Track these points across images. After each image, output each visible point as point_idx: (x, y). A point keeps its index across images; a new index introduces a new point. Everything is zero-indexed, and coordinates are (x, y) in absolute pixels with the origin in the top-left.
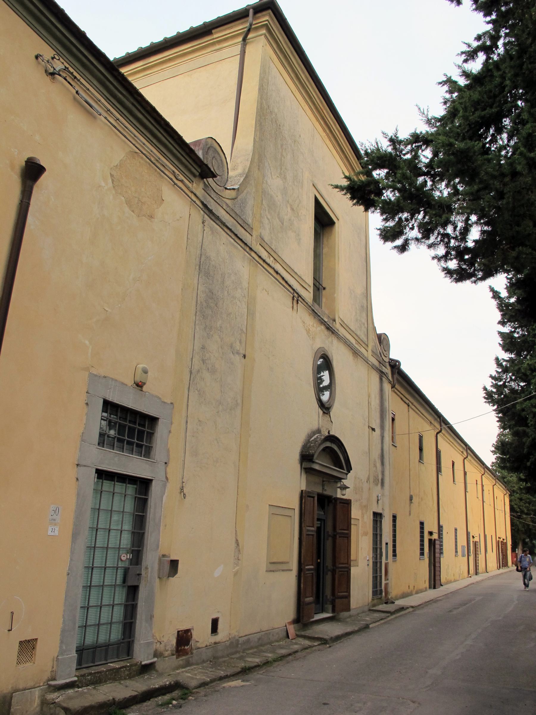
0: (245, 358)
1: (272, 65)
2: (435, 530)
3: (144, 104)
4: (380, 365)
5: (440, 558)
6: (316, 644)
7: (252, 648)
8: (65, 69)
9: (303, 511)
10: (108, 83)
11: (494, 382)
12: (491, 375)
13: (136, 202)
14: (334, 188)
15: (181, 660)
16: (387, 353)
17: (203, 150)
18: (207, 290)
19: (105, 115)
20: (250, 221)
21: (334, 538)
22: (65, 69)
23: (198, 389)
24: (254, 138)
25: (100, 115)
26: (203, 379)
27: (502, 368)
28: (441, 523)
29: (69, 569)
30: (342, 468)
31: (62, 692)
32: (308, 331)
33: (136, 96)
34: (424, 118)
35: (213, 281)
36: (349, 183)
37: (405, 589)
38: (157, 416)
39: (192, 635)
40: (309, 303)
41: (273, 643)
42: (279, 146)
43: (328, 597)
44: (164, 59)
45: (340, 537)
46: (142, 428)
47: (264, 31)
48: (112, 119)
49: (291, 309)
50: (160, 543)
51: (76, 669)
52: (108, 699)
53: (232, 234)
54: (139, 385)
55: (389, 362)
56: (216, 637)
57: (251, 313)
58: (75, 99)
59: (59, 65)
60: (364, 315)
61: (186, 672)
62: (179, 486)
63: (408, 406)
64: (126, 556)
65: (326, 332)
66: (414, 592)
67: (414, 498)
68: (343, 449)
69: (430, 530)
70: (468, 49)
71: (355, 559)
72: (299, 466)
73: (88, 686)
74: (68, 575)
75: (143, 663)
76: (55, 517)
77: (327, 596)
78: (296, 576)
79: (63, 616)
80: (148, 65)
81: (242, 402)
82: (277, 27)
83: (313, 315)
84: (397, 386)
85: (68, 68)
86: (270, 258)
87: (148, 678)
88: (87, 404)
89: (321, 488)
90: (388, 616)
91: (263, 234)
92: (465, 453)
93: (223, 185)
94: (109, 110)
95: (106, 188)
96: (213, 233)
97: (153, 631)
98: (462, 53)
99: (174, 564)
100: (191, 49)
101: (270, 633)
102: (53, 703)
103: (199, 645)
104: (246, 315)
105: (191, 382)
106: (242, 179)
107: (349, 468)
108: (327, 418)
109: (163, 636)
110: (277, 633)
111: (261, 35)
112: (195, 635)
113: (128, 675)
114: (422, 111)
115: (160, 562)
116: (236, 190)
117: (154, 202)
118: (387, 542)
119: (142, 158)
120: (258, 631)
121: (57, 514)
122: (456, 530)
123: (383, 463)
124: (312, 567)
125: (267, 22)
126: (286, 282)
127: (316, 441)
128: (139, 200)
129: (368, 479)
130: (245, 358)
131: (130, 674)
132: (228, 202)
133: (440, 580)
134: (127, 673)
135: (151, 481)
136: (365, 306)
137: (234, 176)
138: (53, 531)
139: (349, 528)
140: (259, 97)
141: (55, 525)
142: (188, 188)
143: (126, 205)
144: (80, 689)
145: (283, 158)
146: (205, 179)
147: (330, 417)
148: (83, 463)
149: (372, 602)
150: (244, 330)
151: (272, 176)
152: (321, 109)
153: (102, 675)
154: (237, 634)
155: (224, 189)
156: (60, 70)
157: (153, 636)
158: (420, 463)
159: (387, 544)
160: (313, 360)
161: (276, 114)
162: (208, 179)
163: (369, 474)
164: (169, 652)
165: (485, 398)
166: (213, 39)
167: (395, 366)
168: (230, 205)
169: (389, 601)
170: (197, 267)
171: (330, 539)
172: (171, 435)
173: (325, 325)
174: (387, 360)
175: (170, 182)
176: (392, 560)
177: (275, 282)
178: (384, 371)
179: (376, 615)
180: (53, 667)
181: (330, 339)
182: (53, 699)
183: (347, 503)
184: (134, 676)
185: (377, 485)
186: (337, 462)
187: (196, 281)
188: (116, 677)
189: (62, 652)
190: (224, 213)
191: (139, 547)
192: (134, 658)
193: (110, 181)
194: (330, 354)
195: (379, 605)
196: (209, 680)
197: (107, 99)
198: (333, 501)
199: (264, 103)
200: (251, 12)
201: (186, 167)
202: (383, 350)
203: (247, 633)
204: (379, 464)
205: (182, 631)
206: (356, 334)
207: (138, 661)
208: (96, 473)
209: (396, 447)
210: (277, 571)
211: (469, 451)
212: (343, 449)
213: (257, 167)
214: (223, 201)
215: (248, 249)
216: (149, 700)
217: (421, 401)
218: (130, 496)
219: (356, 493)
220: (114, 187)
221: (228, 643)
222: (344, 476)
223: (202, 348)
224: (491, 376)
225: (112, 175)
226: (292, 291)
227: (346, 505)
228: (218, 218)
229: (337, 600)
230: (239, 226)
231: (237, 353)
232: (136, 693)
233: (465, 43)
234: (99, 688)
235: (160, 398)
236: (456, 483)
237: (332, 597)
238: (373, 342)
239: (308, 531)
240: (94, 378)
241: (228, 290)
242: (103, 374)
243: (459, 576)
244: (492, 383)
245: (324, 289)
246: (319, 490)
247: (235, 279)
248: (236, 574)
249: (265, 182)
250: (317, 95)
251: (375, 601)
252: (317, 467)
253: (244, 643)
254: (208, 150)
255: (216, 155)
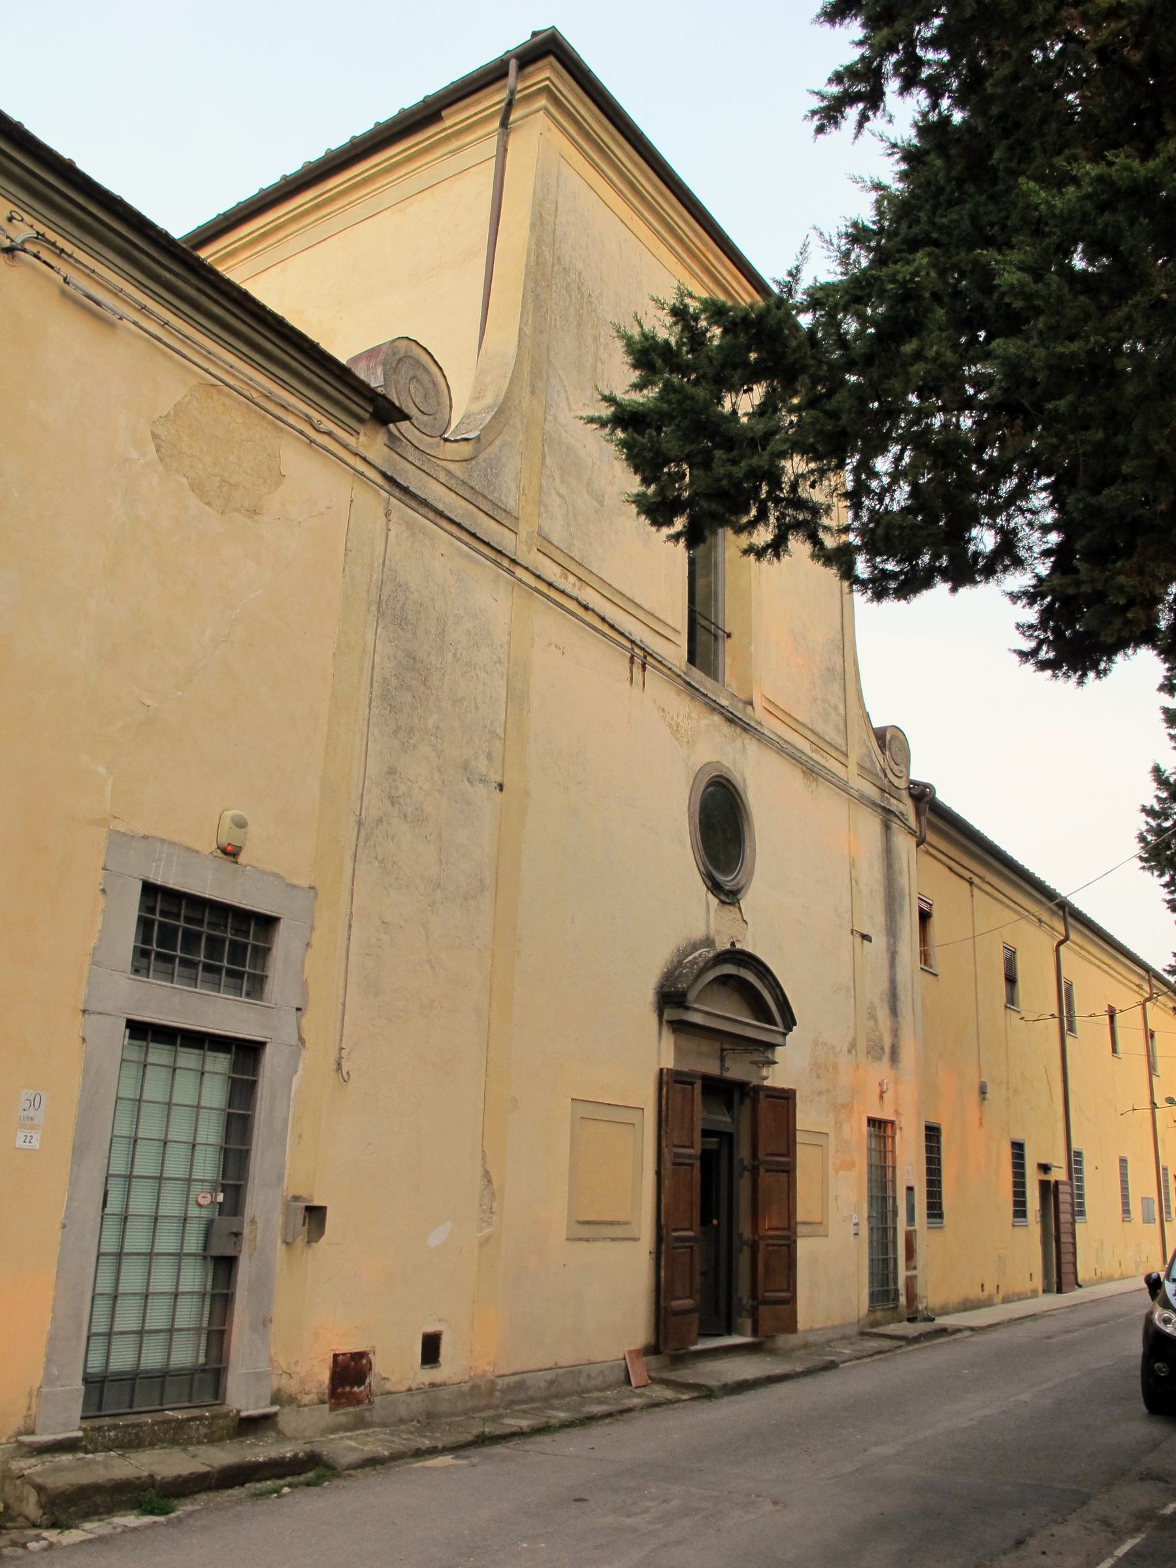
0: (501, 790)
1: (565, 169)
2: (1059, 1161)
3: (222, 286)
4: (883, 796)
5: (1073, 1223)
6: (685, 1397)
7: (532, 1400)
8: (37, 238)
9: (664, 1113)
10: (136, 253)
11: (1153, 823)
12: (1144, 806)
13: (217, 484)
14: (586, 423)
15: (344, 1414)
16: (904, 769)
17: (384, 364)
18: (400, 653)
19: (136, 317)
20: (511, 504)
21: (754, 1171)
22: (37, 238)
23: (380, 857)
24: (520, 329)
25: (121, 319)
26: (393, 838)
27: (1167, 790)
28: (1075, 1146)
29: (66, 1217)
30: (770, 1020)
31: (48, 1457)
32: (675, 730)
33: (204, 273)
34: (835, 254)
35: (415, 634)
36: (613, 409)
37: (974, 1293)
38: (273, 914)
39: (370, 1364)
40: (674, 669)
41: (589, 1391)
42: (590, 340)
43: (745, 1301)
44: (354, 181)
45: (767, 1171)
46: (242, 939)
47: (543, 102)
48: (154, 324)
49: (628, 683)
50: (287, 1171)
51: (82, 1418)
52: (137, 1476)
53: (465, 533)
54: (231, 853)
55: (909, 788)
56: (434, 1371)
57: (517, 697)
58: (64, 293)
59: (21, 232)
60: (836, 687)
61: (350, 1438)
62: (333, 1056)
63: (971, 883)
64: (209, 1196)
65: (727, 729)
66: (998, 1298)
67: (989, 1089)
68: (771, 980)
69: (1043, 1161)
70: (822, 105)
71: (819, 1221)
72: (653, 1018)
73: (111, 1450)
74: (64, 1226)
75: (243, 1414)
76: (31, 1112)
77: (740, 1300)
78: (650, 1253)
79: (53, 1307)
80: (325, 196)
81: (497, 884)
82: (572, 90)
83: (689, 695)
84: (931, 837)
85: (43, 235)
86: (566, 578)
87: (250, 1445)
88: (103, 891)
89: (717, 1063)
90: (900, 1347)
91: (546, 529)
92: (1146, 987)
93: (440, 433)
94: (144, 307)
95: (142, 461)
96: (413, 534)
97: (272, 1351)
98: (814, 113)
99: (315, 1215)
100: (405, 154)
101: (580, 1372)
102: (19, 1477)
103: (388, 1386)
104: (504, 700)
105: (361, 844)
106: (489, 417)
107: (790, 1022)
108: (730, 913)
109: (296, 1363)
110: (602, 1373)
111: (537, 111)
112: (380, 1366)
113: (205, 1436)
114: (827, 238)
115: (287, 1207)
116: (471, 442)
117: (261, 481)
118: (910, 1185)
119: (228, 396)
120: (549, 1366)
121: (36, 1106)
122: (1123, 1161)
123: (894, 1011)
124: (691, 1234)
125: (547, 82)
126: (612, 626)
127: (696, 963)
128: (223, 480)
129: (852, 1048)
130: (501, 790)
131: (213, 1433)
132: (452, 467)
133: (1075, 1273)
134: (203, 1431)
135: (262, 1044)
136: (839, 668)
137: (476, 412)
138: (27, 1141)
139: (790, 1149)
140: (534, 240)
141: (32, 1128)
142: (345, 447)
143: (191, 493)
144: (90, 1456)
145: (599, 365)
146: (391, 426)
147: (740, 910)
148: (92, 1007)
149: (868, 1315)
150: (500, 731)
151: (569, 405)
152: (700, 251)
153: (144, 1432)
154: (489, 1368)
155: (442, 441)
156: (23, 242)
157: (271, 1360)
158: (1008, 1011)
159: (910, 1189)
160: (689, 788)
161: (580, 274)
162: (398, 424)
163: (856, 1033)
164: (313, 1397)
165: (1141, 859)
166: (445, 129)
167: (922, 796)
168: (458, 473)
169: (920, 1316)
170: (374, 608)
171: (746, 1174)
172: (310, 951)
173: (722, 714)
174: (902, 784)
175: (299, 439)
176: (926, 1225)
177: (581, 627)
178: (893, 809)
179: (874, 1344)
180: (29, 1409)
181: (738, 744)
182: (21, 1469)
183: (786, 1098)
184: (221, 1439)
185: (880, 1058)
186: (760, 1011)
187: (370, 637)
188: (177, 1437)
189: (49, 1379)
190: (442, 490)
191: (239, 1180)
192: (227, 1402)
193: (152, 447)
194: (737, 775)
195: (889, 1323)
196: (386, 1453)
197: (140, 286)
198: (751, 1094)
199: (546, 252)
200: (513, 64)
201: (328, 397)
202: (892, 763)
203: (519, 1368)
204: (883, 1013)
205: (344, 1354)
206: (811, 730)
207: (230, 1408)
208: (127, 1027)
209: (936, 975)
210: (594, 1240)
211: (1154, 981)
212: (771, 980)
213: (528, 388)
214: (438, 466)
215: (506, 563)
216: (242, 1485)
217: (1007, 872)
218: (134, 1066)
219: (818, 1077)
220: (161, 459)
221: (465, 1388)
222: (777, 1039)
223: (389, 773)
224: (1144, 809)
225: (155, 436)
226: (629, 645)
227: (785, 1102)
228: (424, 503)
229: (762, 1308)
230: (482, 515)
231: (481, 780)
232: (209, 1469)
233: (814, 92)
234: (133, 1455)
235: (282, 878)
236: (1121, 1055)
237: (750, 1302)
238: (861, 747)
239: (677, 1155)
240: (119, 840)
241: (456, 650)
242: (141, 831)
243: (1137, 1268)
244: (1147, 823)
245: (729, 636)
246: (711, 1068)
247: (475, 627)
248: (485, 1242)
249: (550, 418)
250: (686, 221)
251: (879, 1315)
252: (697, 1019)
253: (509, 1389)
254: (398, 363)
255: (420, 373)
